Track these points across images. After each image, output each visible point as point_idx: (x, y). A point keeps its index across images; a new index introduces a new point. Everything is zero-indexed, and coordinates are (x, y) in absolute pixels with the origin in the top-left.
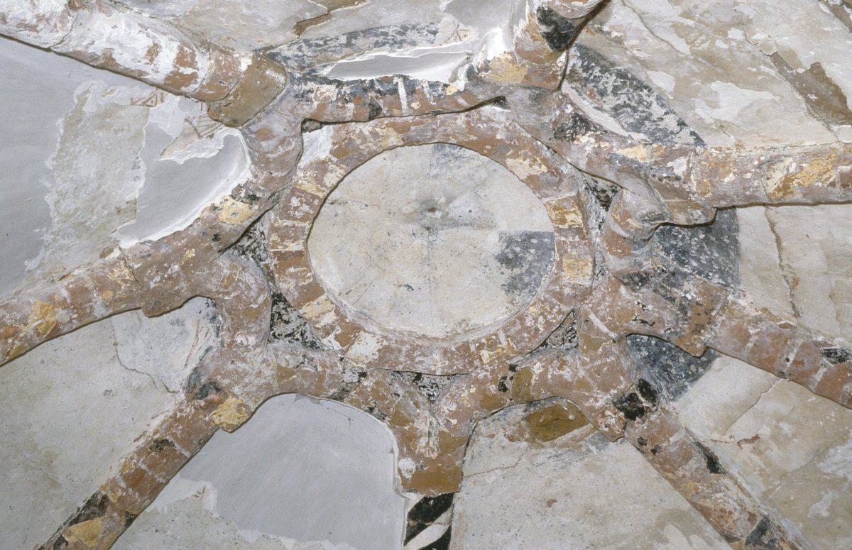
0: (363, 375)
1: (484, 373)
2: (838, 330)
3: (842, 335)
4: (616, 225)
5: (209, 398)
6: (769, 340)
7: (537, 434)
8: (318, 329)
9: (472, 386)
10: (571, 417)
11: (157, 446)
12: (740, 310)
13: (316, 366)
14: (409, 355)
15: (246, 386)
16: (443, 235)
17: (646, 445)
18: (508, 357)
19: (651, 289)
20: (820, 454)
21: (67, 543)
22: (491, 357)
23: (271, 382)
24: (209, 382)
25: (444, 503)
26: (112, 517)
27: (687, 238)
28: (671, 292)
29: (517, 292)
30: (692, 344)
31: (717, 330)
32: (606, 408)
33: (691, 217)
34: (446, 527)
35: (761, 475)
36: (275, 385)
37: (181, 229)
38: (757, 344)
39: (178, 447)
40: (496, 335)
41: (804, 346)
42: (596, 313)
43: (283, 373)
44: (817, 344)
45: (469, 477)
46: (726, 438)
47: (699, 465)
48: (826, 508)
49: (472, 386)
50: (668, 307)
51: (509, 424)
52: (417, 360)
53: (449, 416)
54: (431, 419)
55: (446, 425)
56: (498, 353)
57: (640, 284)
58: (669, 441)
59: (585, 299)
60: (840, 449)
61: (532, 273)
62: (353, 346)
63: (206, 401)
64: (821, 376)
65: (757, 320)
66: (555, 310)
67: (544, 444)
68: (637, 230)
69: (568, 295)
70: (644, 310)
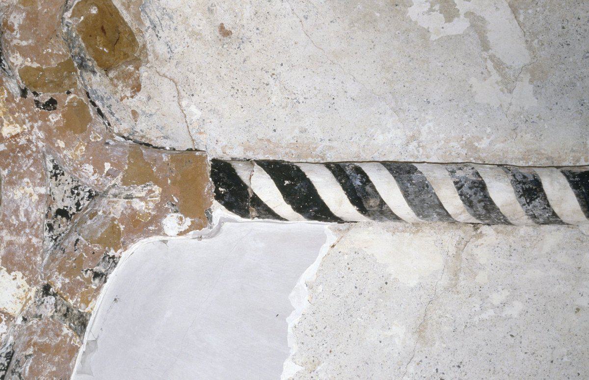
0: (46, 290)
1: (36, 130)
7: (126, 55)
9: (56, 145)
10: (94, 11)
13: (26, 357)
18: (10, 99)
22: (11, 123)
25: (225, 176)
34: (257, 167)
45: (193, 140)
49: (56, 145)
51: (116, 93)
52: (23, 219)
53: (101, 172)
54: (111, 196)
55: (114, 177)
67: (140, 45)
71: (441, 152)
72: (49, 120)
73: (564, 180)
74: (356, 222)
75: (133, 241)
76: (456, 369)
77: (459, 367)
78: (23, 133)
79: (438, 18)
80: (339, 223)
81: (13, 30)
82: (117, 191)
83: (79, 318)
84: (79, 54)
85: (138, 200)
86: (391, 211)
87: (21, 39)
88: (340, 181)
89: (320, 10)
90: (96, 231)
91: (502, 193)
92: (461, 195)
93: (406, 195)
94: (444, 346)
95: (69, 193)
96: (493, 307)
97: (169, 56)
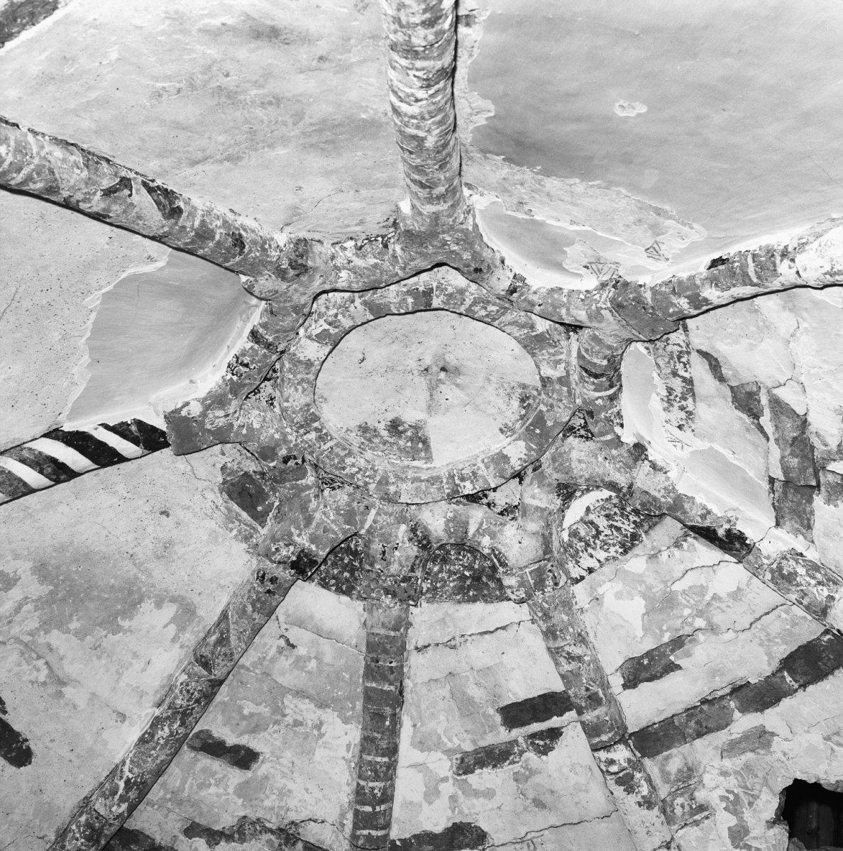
1: (294, 439)
3: (415, 685)
16: (421, 382)
19: (417, 554)
20: (300, 694)
21: (130, 195)
22: (310, 440)
26: (163, 227)
27: (461, 563)
35: (260, 659)
37: (485, 239)
40: (331, 439)
42: (378, 514)
46: (284, 626)
52: (299, 387)
55: (239, 426)
61: (384, 444)
66: (367, 480)
86: (32, 468)
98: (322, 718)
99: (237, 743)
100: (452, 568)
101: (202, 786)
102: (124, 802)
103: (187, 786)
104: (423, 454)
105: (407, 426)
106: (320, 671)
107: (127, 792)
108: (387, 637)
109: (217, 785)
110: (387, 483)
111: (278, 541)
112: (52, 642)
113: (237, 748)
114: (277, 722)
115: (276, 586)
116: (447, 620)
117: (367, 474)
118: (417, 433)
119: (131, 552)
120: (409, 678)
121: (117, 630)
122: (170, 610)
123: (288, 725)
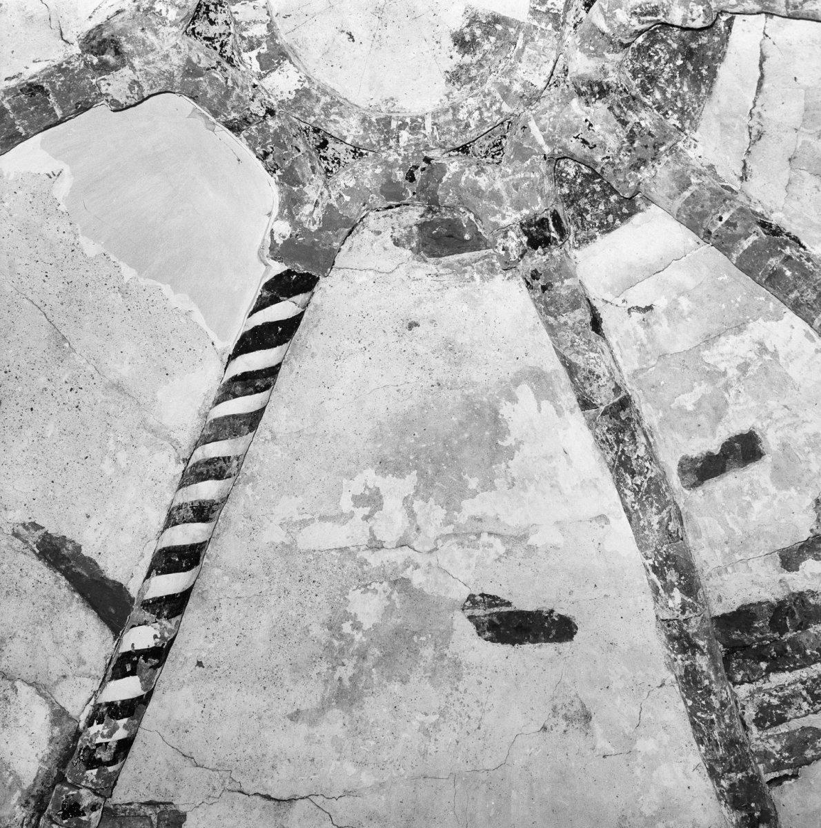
0: (271, 112)
1: (396, 156)
2: (781, 203)
3: (783, 210)
4: (601, 16)
5: (104, 57)
6: (708, 194)
8: (243, 38)
10: (467, 237)
11: (30, 90)
12: (687, 159)
13: (227, 78)
14: (326, 110)
15: (148, 63)
17: (538, 279)
18: (427, 148)
19: (607, 106)
20: (709, 340)
22: (409, 141)
23: (176, 73)
24: (111, 38)
25: (306, 284)
27: (663, 62)
28: (625, 114)
29: (457, 85)
30: (625, 182)
31: (658, 170)
32: (511, 228)
33: (690, 15)
34: (300, 310)
36: (178, 79)
38: (695, 194)
39: (52, 99)
40: (423, 119)
41: (741, 210)
42: (538, 120)
43: (192, 70)
44: (755, 213)
45: (340, 269)
46: (619, 301)
47: (584, 318)
48: (693, 401)
50: (617, 130)
52: (332, 118)
56: (418, 139)
57: (597, 96)
58: (563, 283)
59: (531, 104)
60: (733, 339)
61: (481, 66)
62: (272, 74)
63: (100, 60)
64: (749, 244)
65: (700, 174)
66: (494, 108)
67: (428, 259)
68: (622, 25)
69: (516, 92)
70: (589, 129)
71: (255, 454)
72: (399, 170)
73: (200, 540)
74: (226, 369)
75: (281, 192)
76: (76, 404)
77: (77, 407)
78: (398, 146)
79: (359, 490)
80: (230, 355)
81: (476, 175)
82: (324, 197)
83: (238, 127)
84: (440, 212)
85: (312, 210)
87: (467, 178)
88: (265, 370)
89: (400, 403)
90: (300, 167)
91: (207, 490)
92: (218, 458)
93: (234, 416)
94: (99, 401)
95: (337, 155)
96: (116, 451)
97: (412, 277)
98: (757, 339)
99: (721, 442)
100: (666, 77)
101: (744, 511)
102: (672, 590)
103: (731, 525)
104: (511, 30)
105: (467, 30)
106: (699, 302)
107: (664, 579)
108: (687, 202)
109: (756, 498)
110: (508, 89)
111: (495, 242)
112: (473, 513)
113: (728, 447)
114: (727, 387)
115: (542, 277)
116: (727, 121)
117: (488, 105)
118: (481, 22)
119: (434, 383)
120: (772, 212)
121: (510, 453)
122: (525, 392)
123: (739, 379)
